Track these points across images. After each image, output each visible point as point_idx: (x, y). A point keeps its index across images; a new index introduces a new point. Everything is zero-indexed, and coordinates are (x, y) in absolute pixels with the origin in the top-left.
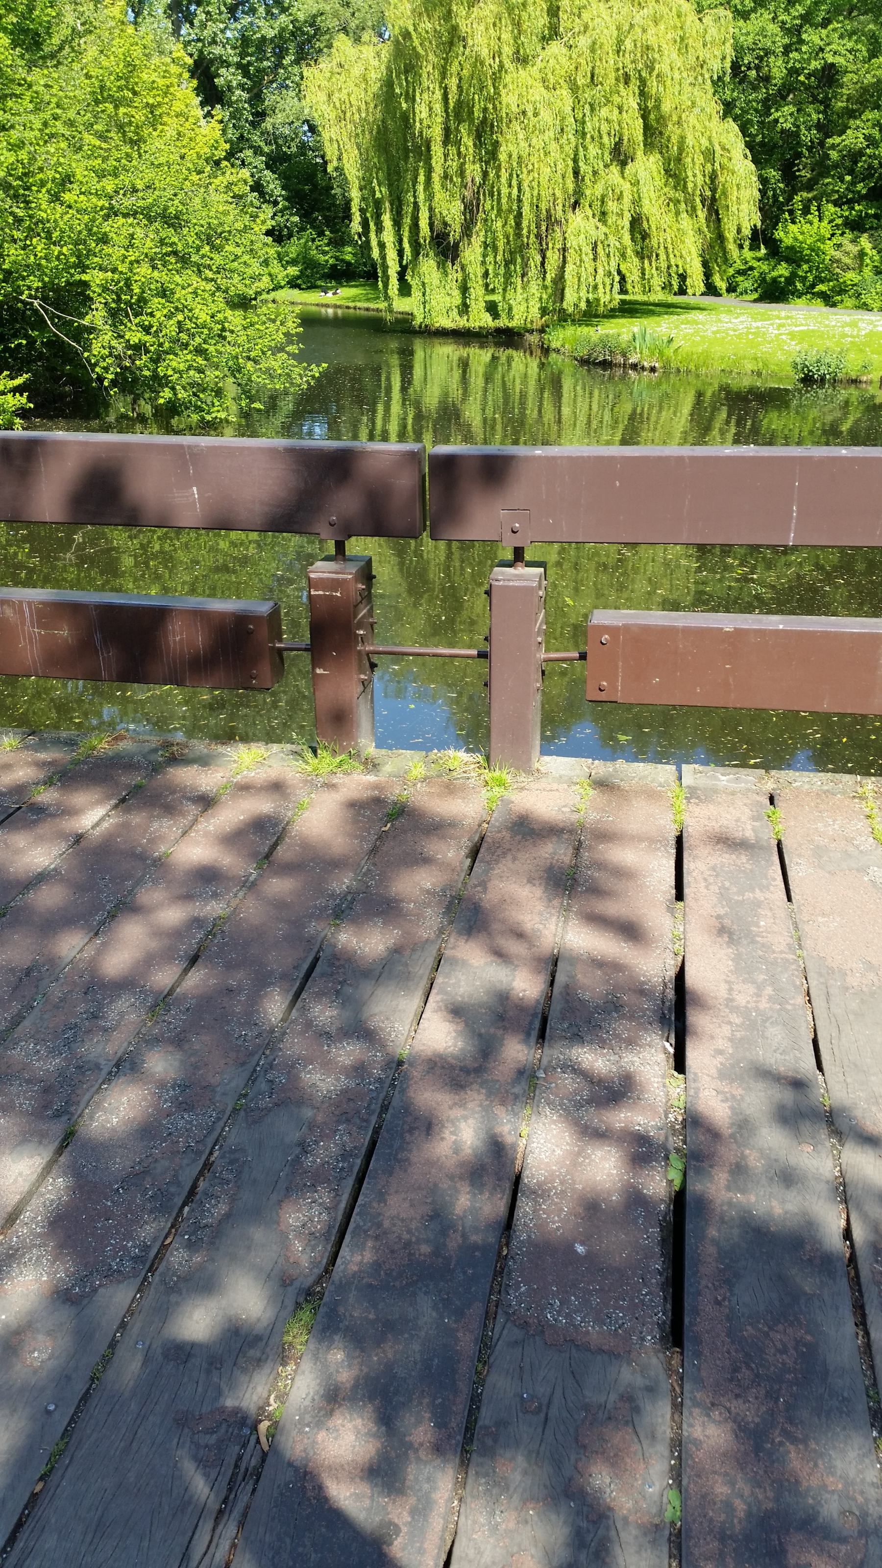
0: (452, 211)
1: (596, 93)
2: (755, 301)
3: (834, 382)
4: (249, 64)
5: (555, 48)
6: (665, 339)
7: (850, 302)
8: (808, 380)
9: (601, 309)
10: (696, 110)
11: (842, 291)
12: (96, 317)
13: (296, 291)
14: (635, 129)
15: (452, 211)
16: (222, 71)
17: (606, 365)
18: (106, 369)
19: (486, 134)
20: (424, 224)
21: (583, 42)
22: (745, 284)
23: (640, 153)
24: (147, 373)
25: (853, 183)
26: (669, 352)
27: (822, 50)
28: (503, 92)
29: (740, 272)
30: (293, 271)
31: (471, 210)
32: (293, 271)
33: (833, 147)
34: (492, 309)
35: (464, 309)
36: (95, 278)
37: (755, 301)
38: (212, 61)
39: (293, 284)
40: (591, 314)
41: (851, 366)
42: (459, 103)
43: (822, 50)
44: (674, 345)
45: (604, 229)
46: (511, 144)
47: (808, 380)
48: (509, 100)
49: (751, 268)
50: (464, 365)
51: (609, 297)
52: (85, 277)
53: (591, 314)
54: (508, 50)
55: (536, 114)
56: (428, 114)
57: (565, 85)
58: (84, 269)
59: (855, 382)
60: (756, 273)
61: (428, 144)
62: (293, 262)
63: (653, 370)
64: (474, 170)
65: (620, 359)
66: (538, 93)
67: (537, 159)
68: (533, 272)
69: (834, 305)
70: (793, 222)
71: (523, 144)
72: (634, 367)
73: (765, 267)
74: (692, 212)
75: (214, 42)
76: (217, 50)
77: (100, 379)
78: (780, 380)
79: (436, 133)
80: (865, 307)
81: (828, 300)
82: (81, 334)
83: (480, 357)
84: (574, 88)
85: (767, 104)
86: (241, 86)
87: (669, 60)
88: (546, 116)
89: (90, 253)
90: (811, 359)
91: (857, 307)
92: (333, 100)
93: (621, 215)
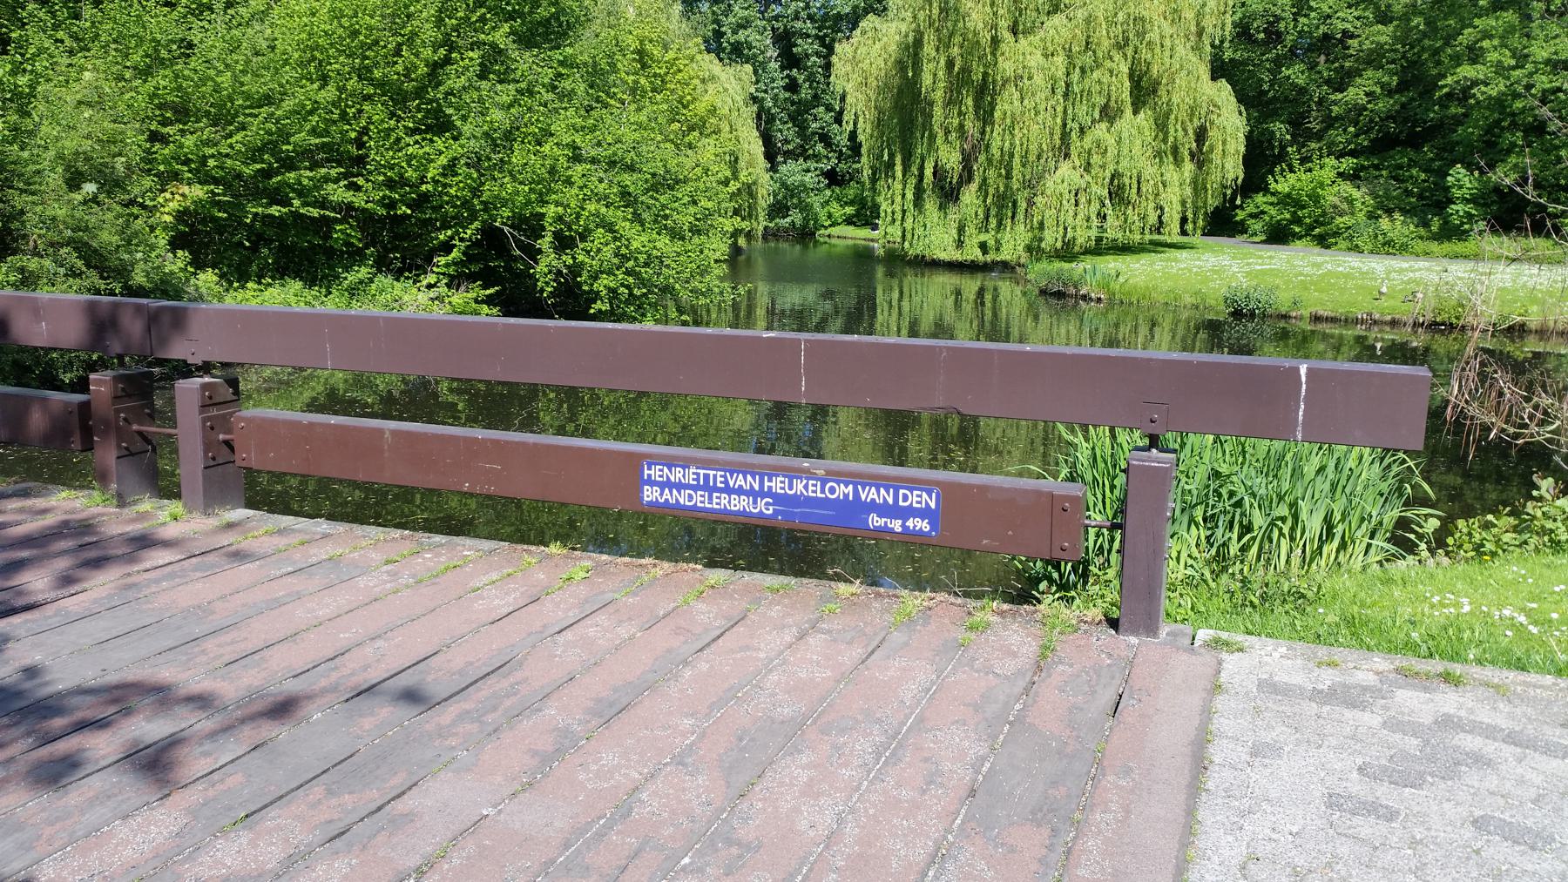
0: (951, 159)
1: (1088, 59)
2: (1262, 242)
3: (1264, 316)
4: (826, 35)
5: (1058, 20)
6: (1113, 273)
7: (1343, 244)
8: (1237, 314)
9: (1077, 249)
10: (1184, 73)
11: (1336, 234)
12: (545, 243)
13: (851, 228)
14: (1123, 90)
15: (951, 159)
16: (799, 41)
17: (1060, 295)
18: (547, 283)
19: (985, 95)
20: (929, 172)
21: (1081, 14)
22: (1256, 225)
23: (1128, 111)
24: (586, 288)
25: (1357, 135)
26: (1115, 286)
27: (1329, 17)
28: (1000, 59)
29: (1252, 216)
30: (849, 210)
31: (967, 161)
32: (849, 210)
33: (1335, 103)
34: (983, 247)
35: (960, 244)
36: (551, 211)
37: (1262, 242)
38: (794, 34)
39: (849, 221)
40: (1067, 252)
41: (1283, 301)
42: (963, 70)
43: (1329, 17)
44: (1121, 279)
45: (1088, 178)
46: (1007, 104)
47: (1237, 314)
48: (1006, 66)
49: (1263, 212)
50: (958, 293)
51: (1083, 236)
52: (543, 210)
53: (1067, 252)
54: (1004, 24)
55: (1030, 78)
56: (933, 78)
57: (1061, 52)
58: (544, 203)
59: (1285, 317)
60: (1267, 218)
61: (931, 104)
62: (851, 203)
63: (1099, 300)
64: (972, 127)
65: (1072, 290)
66: (1036, 59)
67: (1026, 118)
68: (1020, 216)
69: (1328, 247)
70: (1292, 171)
71: (1017, 103)
72: (1084, 298)
73: (1273, 212)
74: (1178, 162)
75: (797, 18)
76: (798, 25)
77: (542, 290)
78: (1217, 313)
79: (938, 96)
80: (1356, 249)
81: (1323, 241)
82: (534, 254)
83: (970, 285)
84: (1069, 54)
85: (1278, 62)
86: (818, 54)
87: (1160, 28)
88: (1039, 79)
89: (550, 191)
90: (1240, 296)
91: (1350, 249)
92: (861, 65)
93: (1103, 167)
